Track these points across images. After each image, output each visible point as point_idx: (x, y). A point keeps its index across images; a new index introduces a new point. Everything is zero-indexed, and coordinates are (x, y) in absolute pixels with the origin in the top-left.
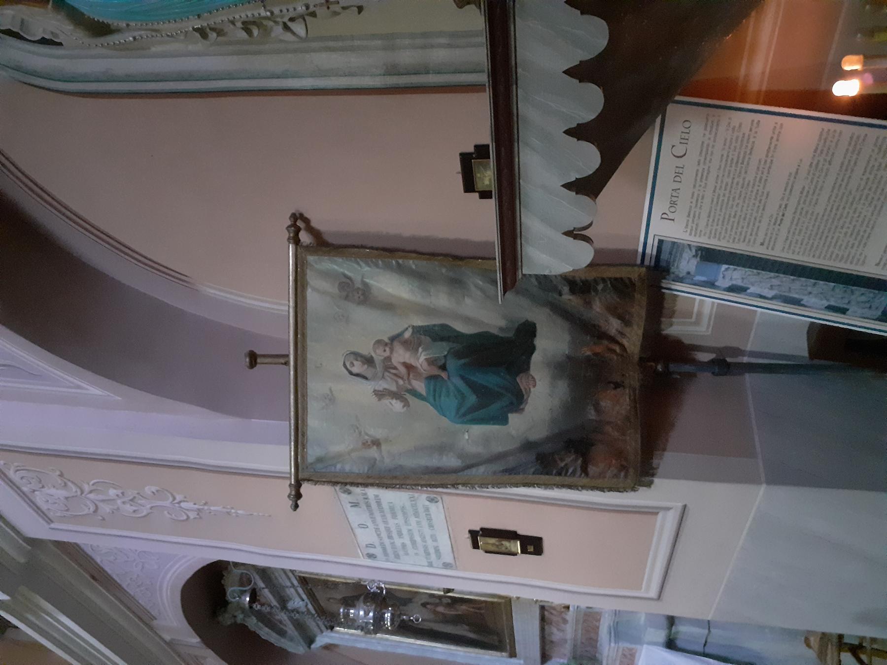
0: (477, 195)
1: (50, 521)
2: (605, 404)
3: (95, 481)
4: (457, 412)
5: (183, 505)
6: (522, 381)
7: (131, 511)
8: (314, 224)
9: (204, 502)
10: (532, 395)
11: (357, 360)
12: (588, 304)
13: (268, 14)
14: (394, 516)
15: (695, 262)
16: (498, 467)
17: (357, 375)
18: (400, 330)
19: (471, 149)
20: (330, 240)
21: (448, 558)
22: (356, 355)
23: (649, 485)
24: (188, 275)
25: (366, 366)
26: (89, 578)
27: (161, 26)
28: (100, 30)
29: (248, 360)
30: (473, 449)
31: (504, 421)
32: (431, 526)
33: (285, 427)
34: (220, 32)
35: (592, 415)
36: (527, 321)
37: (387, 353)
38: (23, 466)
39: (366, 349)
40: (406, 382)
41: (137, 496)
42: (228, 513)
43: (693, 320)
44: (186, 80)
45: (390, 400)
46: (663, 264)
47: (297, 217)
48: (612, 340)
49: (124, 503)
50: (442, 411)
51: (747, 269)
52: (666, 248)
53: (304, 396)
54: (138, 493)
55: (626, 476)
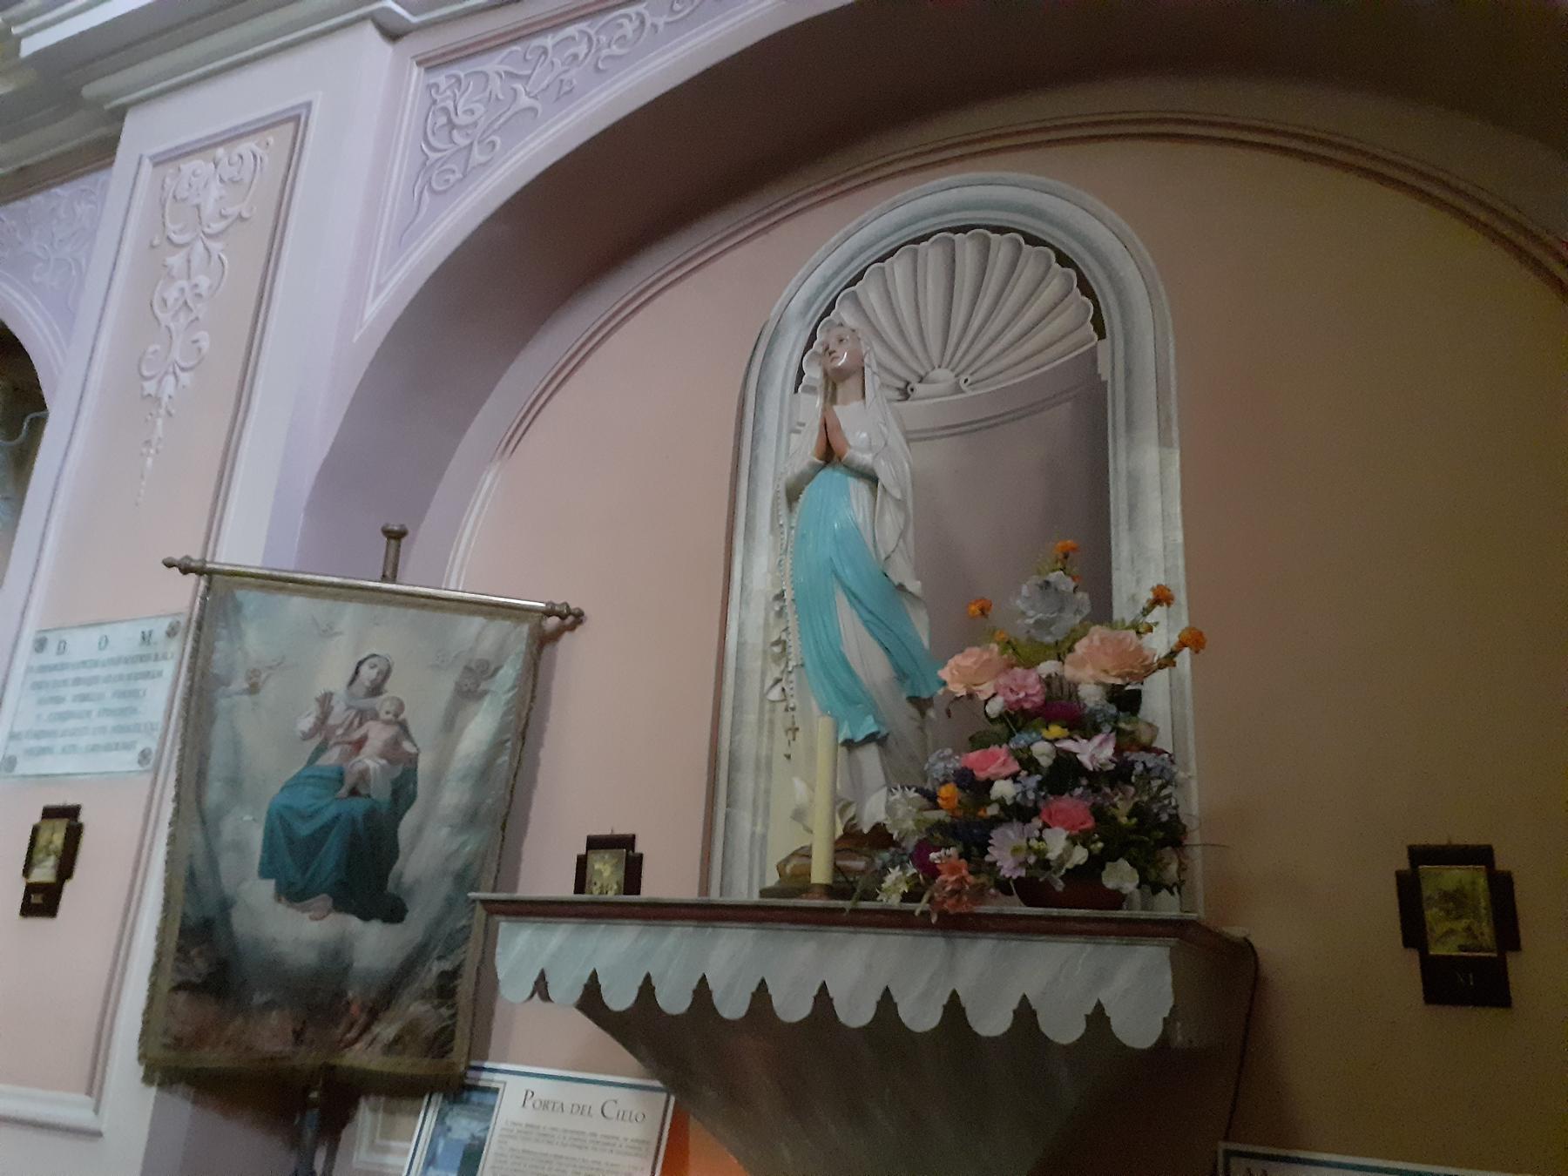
0: (583, 851)
1: (159, 161)
2: (274, 1018)
3: (226, 262)
5: (171, 379)
7: (166, 295)
8: (567, 635)
9: (173, 411)
11: (378, 673)
12: (424, 996)
13: (790, 669)
14: (122, 695)
16: (200, 864)
17: (357, 672)
19: (638, 849)
20: (547, 650)
21: (25, 767)
22: (386, 674)
23: (148, 1079)
24: (514, 454)
26: (23, 163)
27: (789, 556)
28: (793, 495)
29: (396, 528)
30: (228, 829)
31: (265, 873)
32: (94, 748)
33: (286, 564)
34: (780, 613)
35: (259, 999)
36: (407, 911)
37: (383, 716)
38: (262, 169)
39: (392, 688)
40: (340, 740)
41: (192, 317)
42: (148, 443)
44: (746, 525)
46: (465, 1095)
47: (579, 617)
48: (366, 1028)
49: (182, 290)
50: (291, 786)
52: (488, 1098)
53: (336, 597)
54: (197, 319)
55: (165, 1046)
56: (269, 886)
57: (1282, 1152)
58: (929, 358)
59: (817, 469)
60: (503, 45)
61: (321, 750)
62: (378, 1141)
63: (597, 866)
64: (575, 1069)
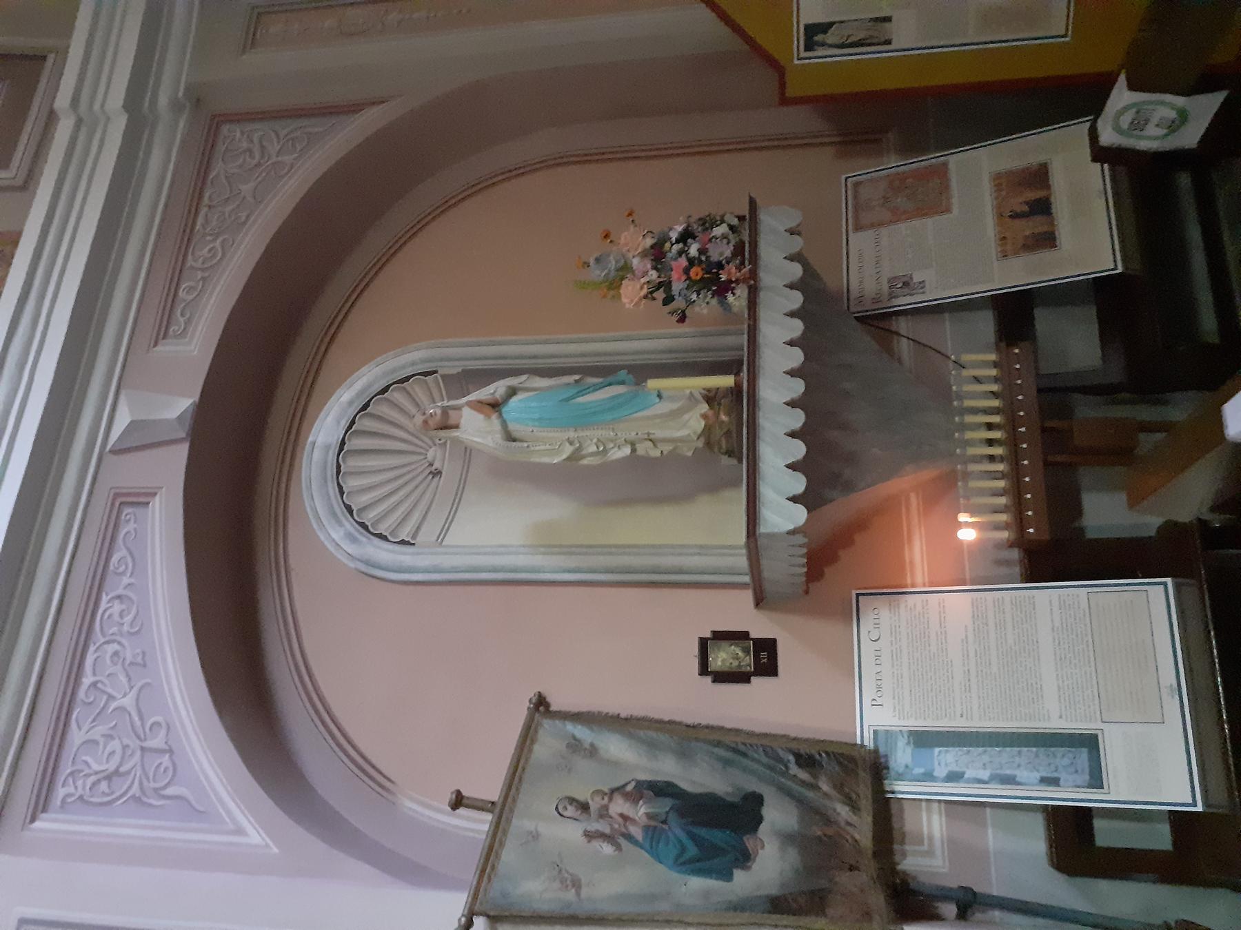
4: (676, 860)
6: (749, 842)
10: (760, 855)
15: (909, 750)
18: (622, 783)
19: (708, 635)
22: (572, 800)
25: (579, 812)
31: (728, 877)
39: (582, 795)
43: (925, 847)
45: (601, 844)
51: (957, 749)
53: (505, 832)
56: (738, 874)
57: (845, 294)
58: (421, 460)
59: (500, 415)
60: (66, 724)
61: (629, 837)
62: (925, 847)
63: (719, 663)
64: (854, 677)
